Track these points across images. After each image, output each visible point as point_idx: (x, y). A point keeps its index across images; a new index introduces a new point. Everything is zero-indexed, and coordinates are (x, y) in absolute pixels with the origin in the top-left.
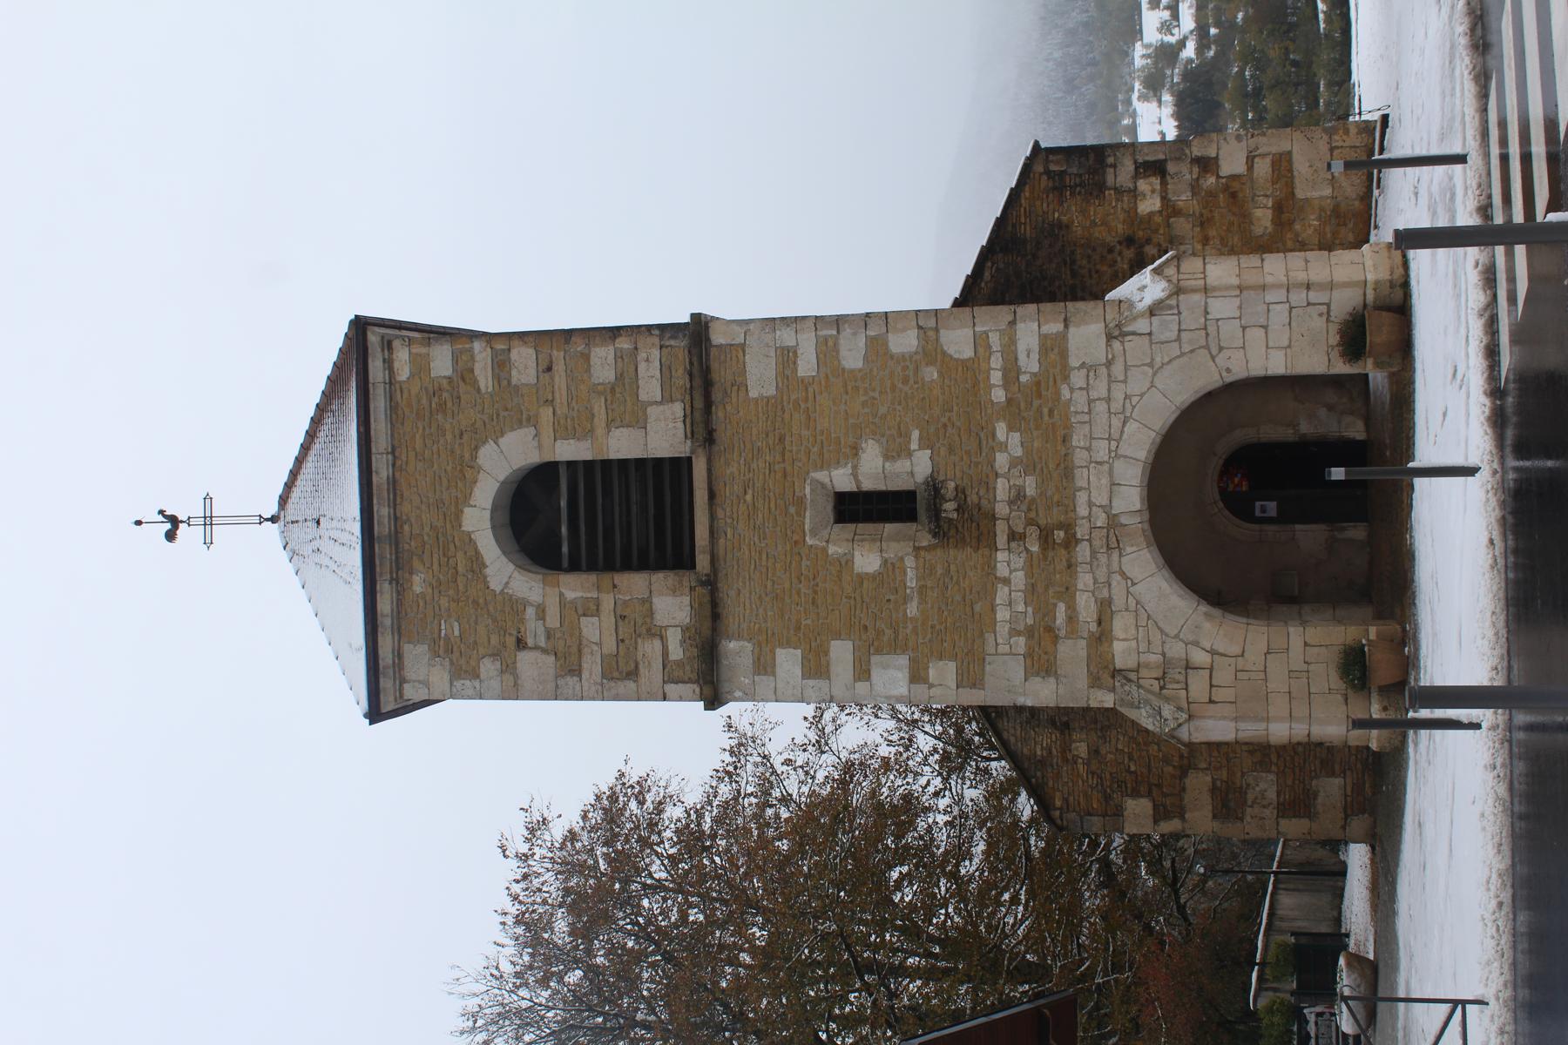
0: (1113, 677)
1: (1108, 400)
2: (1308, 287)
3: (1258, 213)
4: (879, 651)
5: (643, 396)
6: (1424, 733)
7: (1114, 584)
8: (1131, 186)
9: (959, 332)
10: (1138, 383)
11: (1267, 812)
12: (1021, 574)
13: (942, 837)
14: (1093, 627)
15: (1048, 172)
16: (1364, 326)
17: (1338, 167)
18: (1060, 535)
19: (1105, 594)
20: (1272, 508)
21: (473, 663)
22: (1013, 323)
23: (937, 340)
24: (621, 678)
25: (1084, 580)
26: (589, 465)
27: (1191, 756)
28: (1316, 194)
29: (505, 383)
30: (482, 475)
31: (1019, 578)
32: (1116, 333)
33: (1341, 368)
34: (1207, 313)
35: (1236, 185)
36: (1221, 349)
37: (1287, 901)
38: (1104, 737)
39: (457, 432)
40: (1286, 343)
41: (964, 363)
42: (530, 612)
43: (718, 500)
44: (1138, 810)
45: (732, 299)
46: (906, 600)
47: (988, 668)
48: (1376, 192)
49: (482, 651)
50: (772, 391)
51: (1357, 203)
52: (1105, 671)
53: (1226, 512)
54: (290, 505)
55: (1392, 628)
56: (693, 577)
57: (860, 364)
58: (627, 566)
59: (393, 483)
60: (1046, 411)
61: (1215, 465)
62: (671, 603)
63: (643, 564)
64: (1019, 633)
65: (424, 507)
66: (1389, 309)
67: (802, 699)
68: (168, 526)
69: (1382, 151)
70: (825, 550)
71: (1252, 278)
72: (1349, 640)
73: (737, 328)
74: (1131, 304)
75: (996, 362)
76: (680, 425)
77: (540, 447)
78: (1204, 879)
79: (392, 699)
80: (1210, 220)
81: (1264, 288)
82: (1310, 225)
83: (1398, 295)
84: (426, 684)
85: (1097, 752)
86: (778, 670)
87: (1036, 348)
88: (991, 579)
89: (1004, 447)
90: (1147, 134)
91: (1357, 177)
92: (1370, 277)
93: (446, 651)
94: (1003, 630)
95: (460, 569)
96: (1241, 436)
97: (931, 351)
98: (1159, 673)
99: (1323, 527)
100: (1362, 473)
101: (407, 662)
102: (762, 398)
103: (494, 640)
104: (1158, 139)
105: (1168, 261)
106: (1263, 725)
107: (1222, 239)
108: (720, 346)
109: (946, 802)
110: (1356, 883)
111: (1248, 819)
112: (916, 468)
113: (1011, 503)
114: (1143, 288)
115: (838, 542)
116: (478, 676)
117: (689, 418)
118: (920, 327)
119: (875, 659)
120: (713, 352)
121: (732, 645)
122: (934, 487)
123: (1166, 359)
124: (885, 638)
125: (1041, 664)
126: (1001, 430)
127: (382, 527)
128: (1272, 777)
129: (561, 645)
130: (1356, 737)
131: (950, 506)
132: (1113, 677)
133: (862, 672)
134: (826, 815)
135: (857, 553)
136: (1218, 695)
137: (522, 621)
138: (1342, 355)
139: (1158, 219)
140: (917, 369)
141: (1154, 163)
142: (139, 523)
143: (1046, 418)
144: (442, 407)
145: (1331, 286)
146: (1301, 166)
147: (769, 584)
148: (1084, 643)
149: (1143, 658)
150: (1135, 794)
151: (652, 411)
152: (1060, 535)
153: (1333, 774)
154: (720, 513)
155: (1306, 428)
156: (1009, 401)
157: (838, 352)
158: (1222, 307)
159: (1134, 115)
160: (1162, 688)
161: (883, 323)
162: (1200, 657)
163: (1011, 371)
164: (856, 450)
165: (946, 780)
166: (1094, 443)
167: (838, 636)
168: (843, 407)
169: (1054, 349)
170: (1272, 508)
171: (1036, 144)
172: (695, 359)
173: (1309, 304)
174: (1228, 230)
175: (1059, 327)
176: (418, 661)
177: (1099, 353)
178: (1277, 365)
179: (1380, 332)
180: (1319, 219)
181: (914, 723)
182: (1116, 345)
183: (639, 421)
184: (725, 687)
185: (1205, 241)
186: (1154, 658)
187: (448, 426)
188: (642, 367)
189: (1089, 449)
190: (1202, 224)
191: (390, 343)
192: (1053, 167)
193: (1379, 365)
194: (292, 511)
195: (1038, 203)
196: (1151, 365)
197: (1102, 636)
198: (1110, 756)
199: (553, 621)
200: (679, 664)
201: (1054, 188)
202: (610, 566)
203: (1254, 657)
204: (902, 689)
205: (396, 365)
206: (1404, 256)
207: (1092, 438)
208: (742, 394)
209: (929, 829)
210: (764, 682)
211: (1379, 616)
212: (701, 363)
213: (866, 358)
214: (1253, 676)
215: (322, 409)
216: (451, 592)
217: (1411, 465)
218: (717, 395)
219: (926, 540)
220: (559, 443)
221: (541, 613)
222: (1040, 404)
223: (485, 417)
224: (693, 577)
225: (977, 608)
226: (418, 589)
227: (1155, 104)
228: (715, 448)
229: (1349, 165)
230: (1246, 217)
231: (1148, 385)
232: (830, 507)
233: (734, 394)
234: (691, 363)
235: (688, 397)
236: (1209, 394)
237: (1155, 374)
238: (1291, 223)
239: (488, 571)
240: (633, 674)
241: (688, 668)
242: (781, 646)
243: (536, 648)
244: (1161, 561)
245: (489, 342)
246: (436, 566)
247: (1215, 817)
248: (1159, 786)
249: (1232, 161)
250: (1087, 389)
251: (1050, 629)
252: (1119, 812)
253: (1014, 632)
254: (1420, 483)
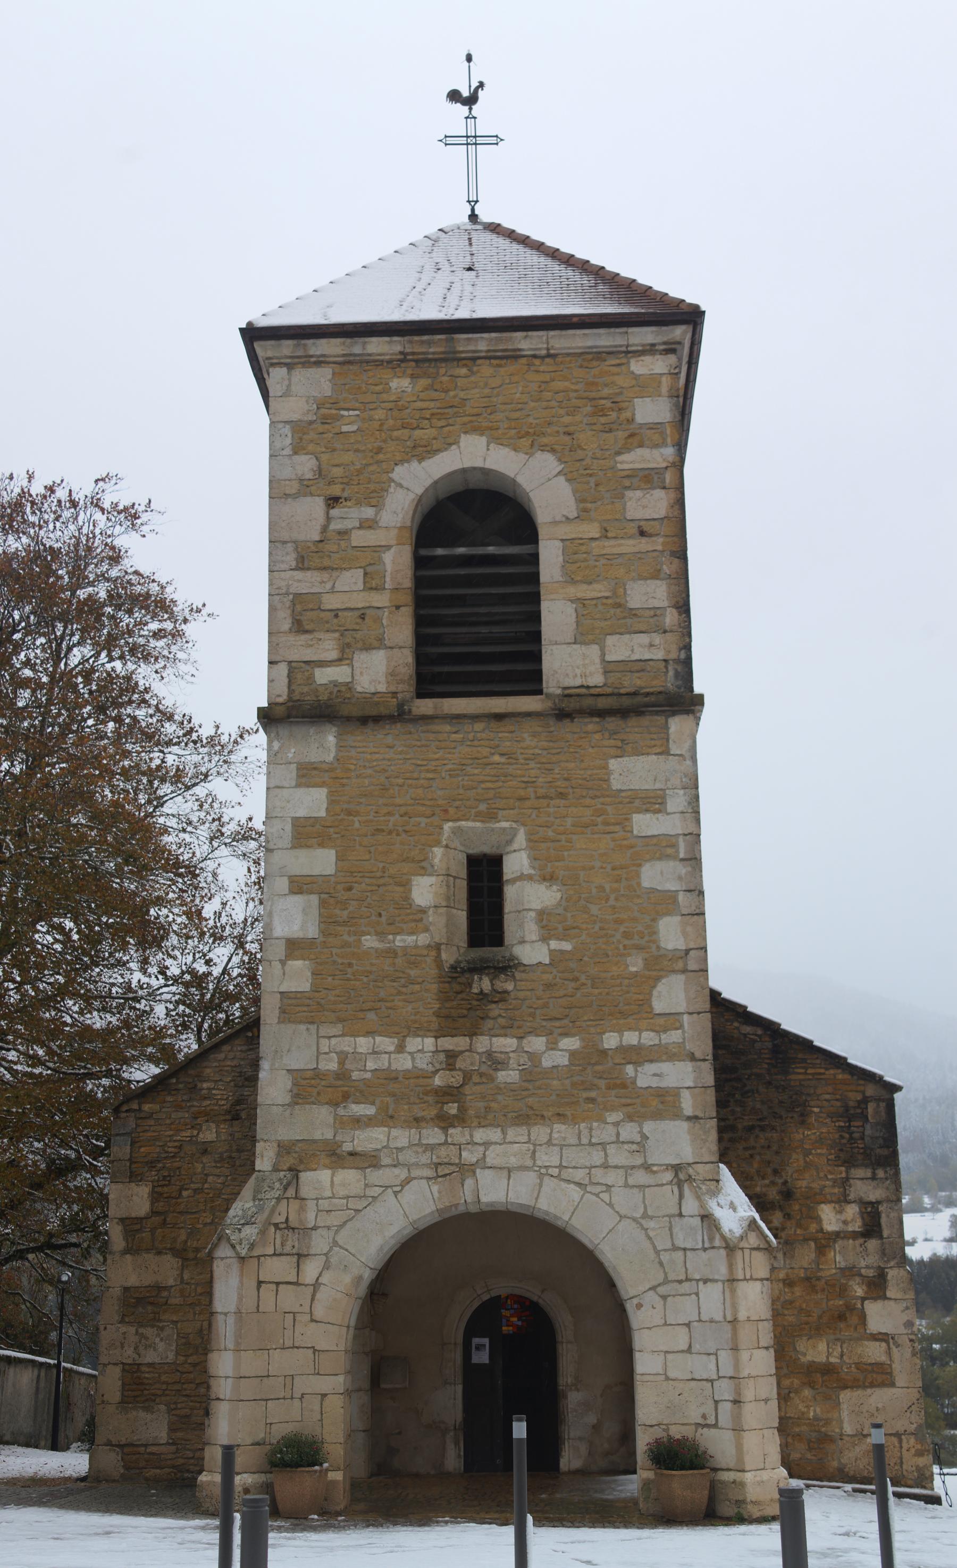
0: (290, 1169)
1: (605, 1166)
2: (736, 1402)
3: (822, 1346)
4: (323, 904)
5: (610, 640)
6: (215, 1537)
7: (396, 1171)
8: (852, 1197)
9: (682, 996)
10: (624, 1200)
11: (130, 1351)
12: (408, 1065)
13: (116, 977)
14: (348, 1147)
15: (865, 1100)
16: (693, 1467)
17: (877, 1437)
18: (453, 1109)
19: (386, 1161)
20: (482, 1357)
21: (311, 447)
22: (692, 1058)
23: (674, 971)
24: (294, 615)
25: (402, 1137)
26: (534, 578)
27: (198, 1263)
28: (845, 1414)
29: (627, 483)
30: (522, 457)
31: (404, 1063)
32: (682, 1176)
33: (643, 1440)
34: (706, 1281)
35: (854, 1320)
36: (664, 1298)
37: (24, 1380)
38: (222, 1159)
39: (571, 429)
40: (671, 1374)
41: (646, 1002)
42: (369, 512)
43: (494, 724)
44: (135, 1199)
45: (716, 739)
46: (381, 935)
47: (303, 1027)
48: (849, 1487)
49: (324, 457)
50: (616, 784)
51: (835, 1464)
52: (297, 1159)
53: (477, 1304)
54: (489, 236)
55: (341, 1500)
56: (408, 696)
57: (646, 883)
58: (420, 622)
59: (514, 356)
60: (593, 1094)
61: (532, 1291)
62: (378, 671)
63: (421, 641)
64: (342, 1063)
65: (487, 391)
66: (712, 1499)
67: (269, 817)
68: (465, 94)
69: (898, 1495)
70: (438, 843)
71: (746, 1335)
72: (327, 1447)
73: (687, 745)
74: (715, 1192)
75: (649, 1038)
76: (578, 682)
77: (555, 523)
78: (55, 1282)
79: (270, 354)
80: (813, 1289)
81: (735, 1349)
82: (809, 1406)
83: (726, 1509)
84: (287, 394)
85: (205, 1152)
86: (301, 791)
87: (663, 1084)
88: (403, 1031)
89: (552, 1046)
90: (913, 1225)
91: (865, 1465)
92: (749, 1477)
93: (325, 417)
94: (346, 1044)
95: (418, 433)
96: (564, 1322)
97: (661, 964)
98: (293, 1223)
99: (459, 1416)
100: (520, 1459)
101: (313, 372)
102: (609, 773)
103: (337, 472)
104: (907, 1237)
105: (765, 1237)
106: (231, 1346)
107: (791, 1302)
108: (666, 727)
109: (150, 982)
110: (43, 1460)
111: (123, 1329)
112: (529, 946)
113: (489, 1054)
114: (733, 1208)
115: (446, 859)
116: (295, 453)
117: (587, 691)
118: (687, 952)
119: (314, 899)
120: (660, 719)
121: (331, 739)
122: (508, 967)
123: (651, 1234)
124: (337, 911)
125: (308, 1087)
126: (571, 1043)
127: (465, 343)
128: (171, 1356)
129: (330, 547)
130: (214, 1455)
131: (486, 984)
132: (290, 1169)
133: (299, 885)
134: (139, 843)
135: (433, 879)
136: (267, 1293)
137: (359, 503)
138: (658, 1442)
139: (813, 1227)
140: (639, 948)
141: (878, 1225)
142: (469, 58)
143: (585, 1095)
144: (600, 412)
145: (738, 1429)
146: (878, 1398)
147: (400, 781)
148: (329, 1135)
149: (311, 1205)
150: (155, 1197)
151: (593, 651)
152: (453, 1109)
153: (172, 1430)
154: (479, 726)
155: (573, 1399)
156: (604, 1052)
157: (660, 859)
158: (712, 1299)
159: (935, 1209)
160: (276, 1226)
161: (692, 909)
162: (311, 1270)
163: (638, 1055)
164: (548, 878)
165: (176, 980)
166: (557, 1149)
167: (339, 858)
168: (598, 864)
169: (663, 1103)
170: (482, 1357)
171: (897, 1088)
172: (653, 699)
173: (716, 1402)
174: (801, 1310)
175: (688, 1110)
176: (309, 386)
177: (660, 1155)
178: (645, 1364)
179: (684, 1486)
180: (816, 1418)
181: (240, 943)
182: (669, 1176)
183: (584, 635)
184: (284, 731)
185: (789, 1283)
186: (310, 1218)
187: (578, 418)
188: (644, 639)
189: (549, 1143)
190: (808, 1279)
191: (673, 351)
192: (871, 1107)
193: (646, 1485)
194: (484, 239)
195: (830, 1089)
196: (645, 1215)
197: (337, 1157)
198: (199, 1167)
199: (360, 538)
200: (310, 679)
201: (847, 1108)
202: (420, 602)
203: (311, 1335)
204: (281, 930)
205: (648, 359)
206: (774, 1519)
207: (562, 1147)
208: (613, 751)
209: (122, 964)
210: (289, 775)
211: (354, 1485)
212: (647, 705)
213: (653, 890)
214: (288, 1333)
215: (598, 273)
216: (391, 422)
217: (530, 1518)
218: (612, 723)
219: (448, 957)
220: (559, 544)
221: (368, 525)
222: (600, 1086)
223: (588, 461)
224: (408, 696)
225: (371, 1016)
226: (394, 384)
227: (948, 1234)
228: (552, 721)
229: (879, 1450)
230: (816, 1331)
231: (623, 1212)
232: (486, 849)
233: (612, 742)
234: (647, 694)
235: (609, 690)
236: (613, 1285)
237: (634, 1219)
238: (811, 1384)
239: (415, 464)
240: (299, 627)
241: (306, 689)
242: (330, 794)
243: (328, 519)
244: (422, 1226)
245: (673, 464)
246: (419, 404)
247: (126, 1289)
248: (164, 1223)
249: (882, 1316)
250: (618, 1141)
251: (346, 1097)
252: (134, 1177)
253: (343, 1057)
254: (508, 1533)
